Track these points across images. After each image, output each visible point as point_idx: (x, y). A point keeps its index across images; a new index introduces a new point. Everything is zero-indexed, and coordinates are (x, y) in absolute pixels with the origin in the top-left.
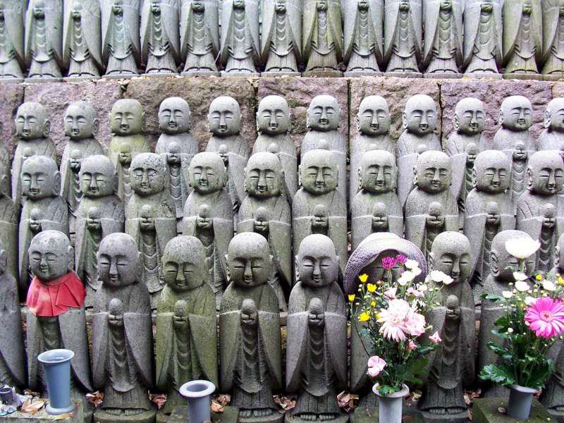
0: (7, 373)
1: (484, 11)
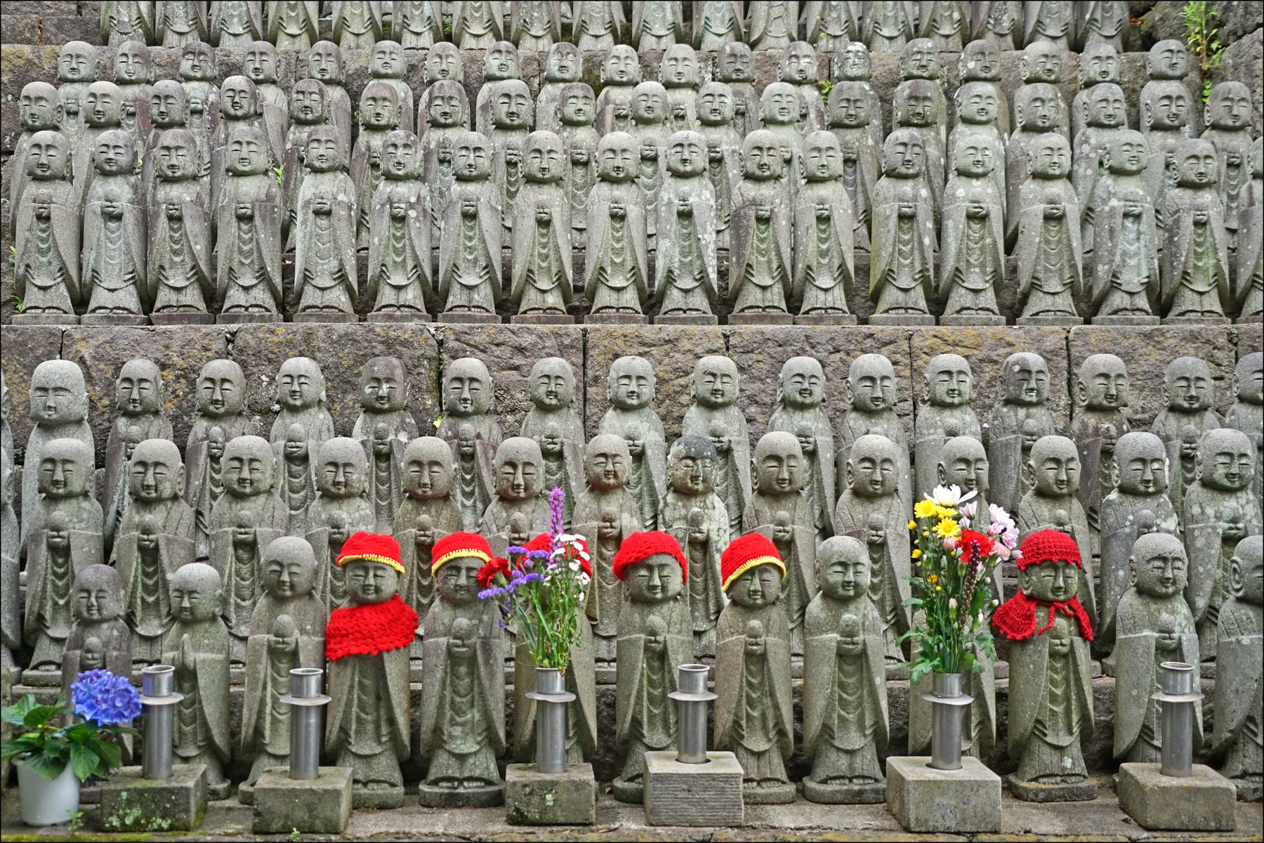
0: (485, 730)
1: (1048, 218)
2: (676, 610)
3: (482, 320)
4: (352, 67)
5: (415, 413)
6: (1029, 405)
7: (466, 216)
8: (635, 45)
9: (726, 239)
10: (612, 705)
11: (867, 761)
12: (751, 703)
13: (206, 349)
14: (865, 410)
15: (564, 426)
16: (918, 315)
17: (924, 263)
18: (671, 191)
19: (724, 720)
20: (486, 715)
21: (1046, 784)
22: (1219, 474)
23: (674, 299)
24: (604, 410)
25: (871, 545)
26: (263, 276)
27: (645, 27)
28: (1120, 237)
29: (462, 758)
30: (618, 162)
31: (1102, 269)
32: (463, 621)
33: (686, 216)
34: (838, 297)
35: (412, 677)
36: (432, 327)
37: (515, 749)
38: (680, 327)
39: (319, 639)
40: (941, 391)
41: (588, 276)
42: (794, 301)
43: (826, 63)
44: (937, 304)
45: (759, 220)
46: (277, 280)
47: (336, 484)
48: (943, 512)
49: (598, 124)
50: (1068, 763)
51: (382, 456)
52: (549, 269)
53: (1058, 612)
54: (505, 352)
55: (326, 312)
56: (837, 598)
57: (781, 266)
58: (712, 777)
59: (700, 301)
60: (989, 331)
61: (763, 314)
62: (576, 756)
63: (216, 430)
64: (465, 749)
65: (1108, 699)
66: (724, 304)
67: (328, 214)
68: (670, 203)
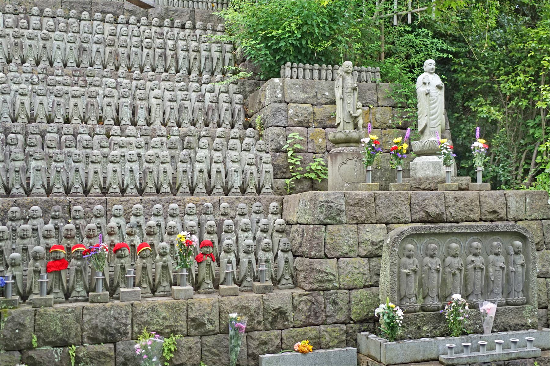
1: (217, 172)
2: (127, 259)
3: (80, 196)
4: (42, 129)
5: (64, 218)
6: (208, 214)
7: (76, 171)
8: (119, 125)
9: (142, 175)
10: (113, 281)
11: (168, 288)
12: (143, 277)
13: (9, 204)
14: (172, 216)
15: (102, 221)
16: (187, 194)
17: (189, 182)
18: (128, 165)
19: (137, 281)
20: (84, 282)
21: (205, 291)
22: (244, 228)
23: (129, 190)
24: (111, 217)
25: (171, 244)
26: (22, 185)
27: (122, 119)
28: (233, 176)
29: (79, 292)
30: (115, 158)
31: (230, 183)
32: (79, 263)
33: (131, 171)
34: (169, 190)
35: (67, 277)
36: (68, 198)
37: (91, 289)
38: (130, 197)
39: (45, 268)
40: (189, 212)
41: (107, 185)
42: (158, 191)
43: (169, 131)
44: (192, 191)
45: (150, 172)
46: (26, 186)
47: (47, 235)
48: (182, 236)
49: (109, 147)
50: (209, 286)
51: (57, 229)
52: (97, 184)
53: (208, 256)
54: (87, 204)
55: (39, 195)
56: (162, 255)
57: (155, 183)
58: (134, 291)
59: (135, 191)
60: (202, 198)
61: (150, 194)
62: (105, 290)
63: (14, 223)
64: (79, 290)
65: (218, 274)
66: (141, 192)
67: (40, 170)
68: (128, 168)
